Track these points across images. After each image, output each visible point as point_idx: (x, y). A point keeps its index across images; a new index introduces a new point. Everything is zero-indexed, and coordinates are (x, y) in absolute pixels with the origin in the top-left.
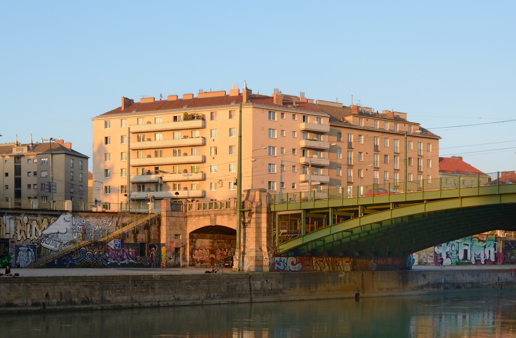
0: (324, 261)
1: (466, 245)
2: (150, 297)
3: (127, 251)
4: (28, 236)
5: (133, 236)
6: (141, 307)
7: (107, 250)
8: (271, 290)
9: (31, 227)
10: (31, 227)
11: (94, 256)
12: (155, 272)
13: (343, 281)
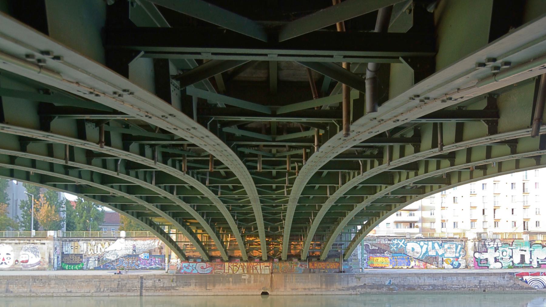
0: (238, 266)
1: (522, 250)
2: (45, 290)
3: (154, 260)
4: (95, 252)
5: (159, 250)
6: (37, 297)
7: (140, 259)
8: (163, 287)
9: (97, 247)
10: (97, 247)
11: (129, 263)
12: (146, 273)
13: (246, 281)
